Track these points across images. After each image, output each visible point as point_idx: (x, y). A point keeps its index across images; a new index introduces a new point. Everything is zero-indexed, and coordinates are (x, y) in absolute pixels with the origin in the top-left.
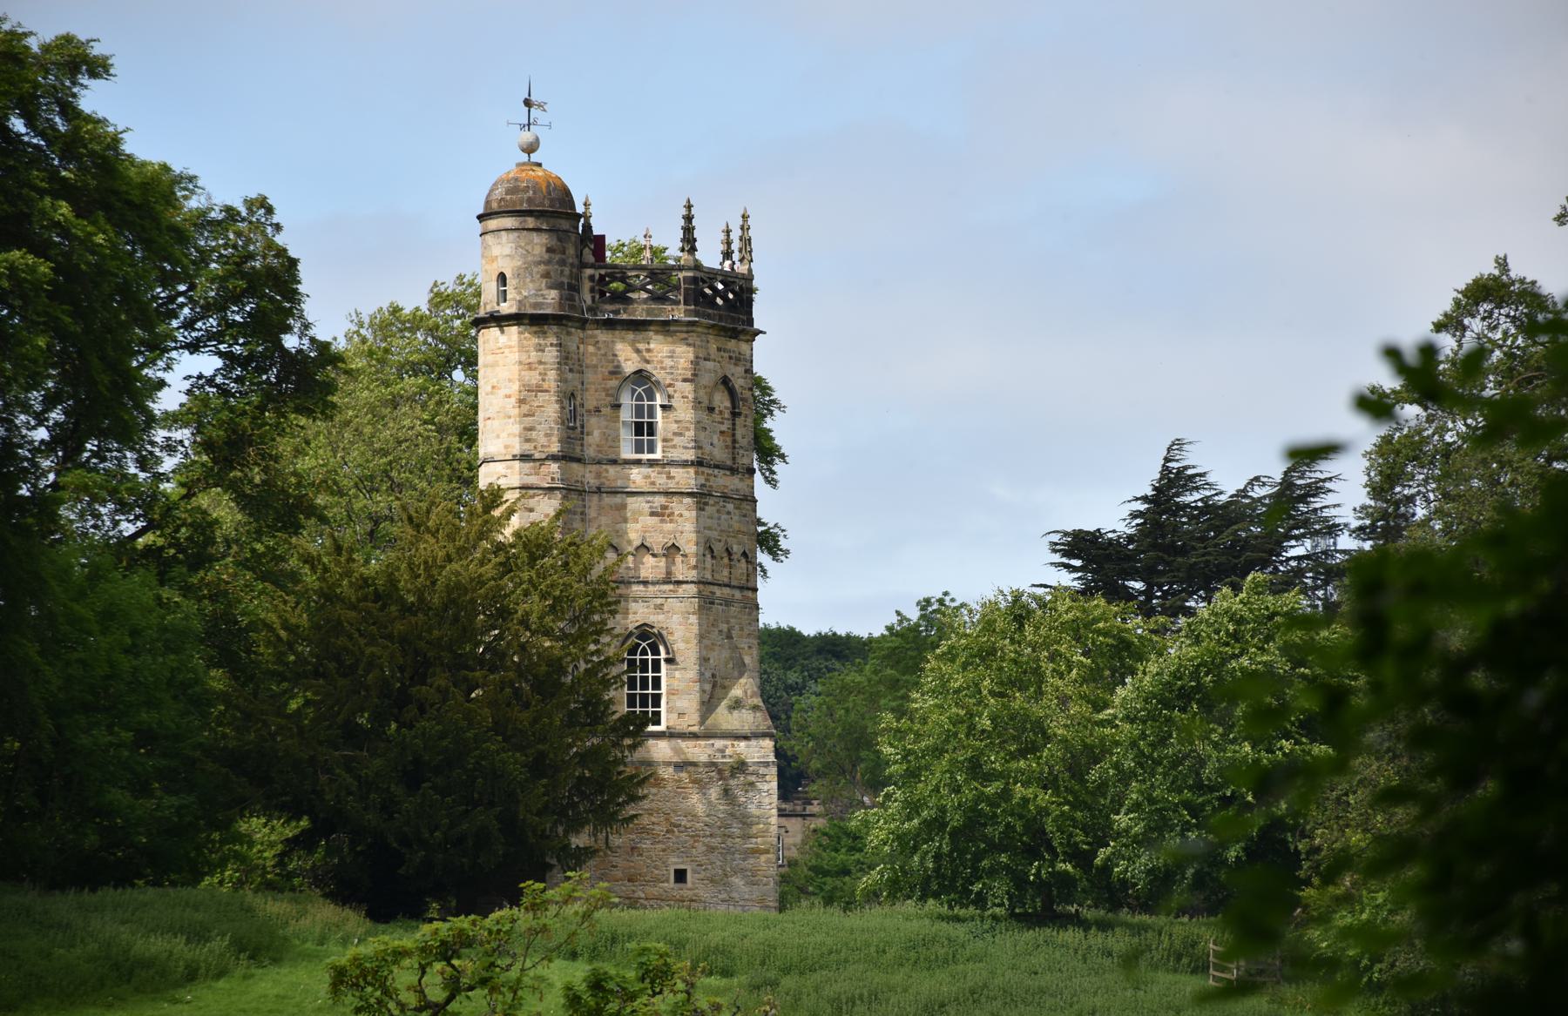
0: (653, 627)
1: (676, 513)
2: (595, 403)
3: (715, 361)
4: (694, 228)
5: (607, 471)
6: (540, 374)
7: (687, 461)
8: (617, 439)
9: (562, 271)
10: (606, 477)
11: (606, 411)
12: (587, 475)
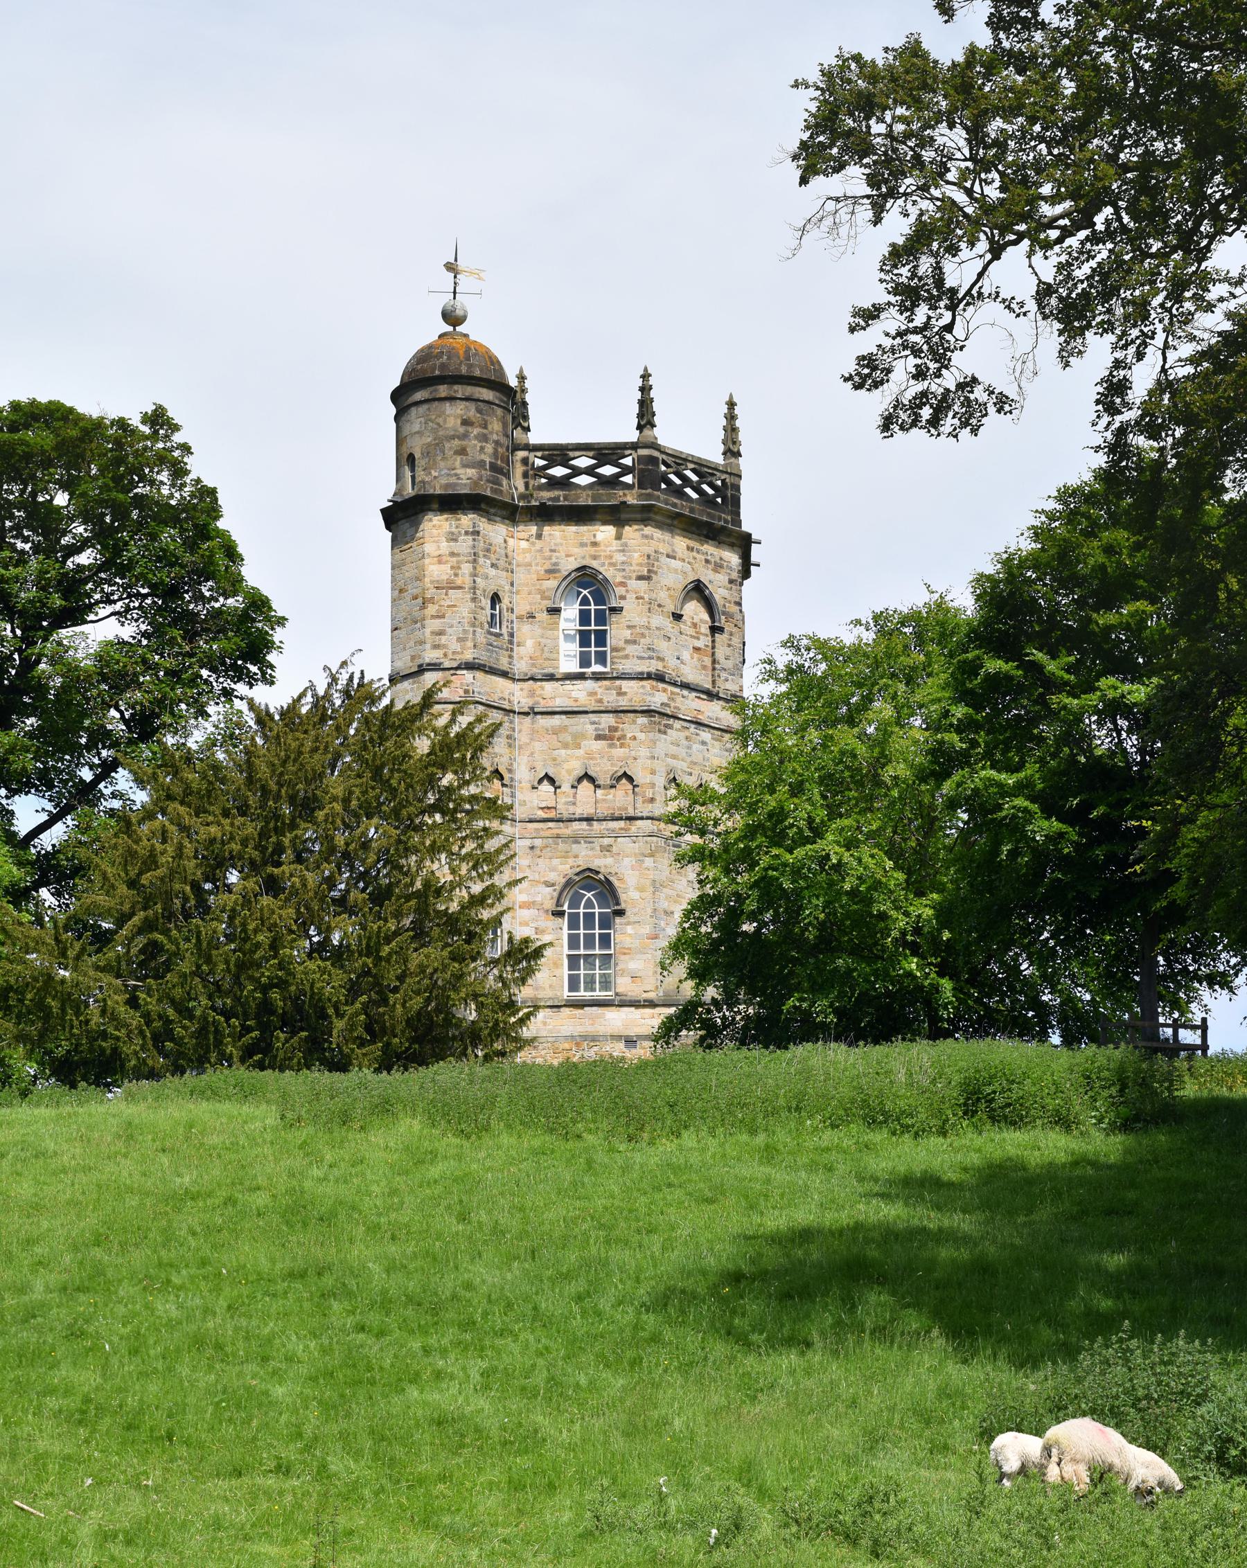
0: (598, 873)
1: (629, 735)
2: (528, 608)
3: (683, 560)
4: (652, 400)
5: (543, 688)
6: (452, 568)
7: (642, 673)
8: (555, 649)
9: (482, 448)
10: (540, 695)
11: (543, 616)
12: (518, 694)
